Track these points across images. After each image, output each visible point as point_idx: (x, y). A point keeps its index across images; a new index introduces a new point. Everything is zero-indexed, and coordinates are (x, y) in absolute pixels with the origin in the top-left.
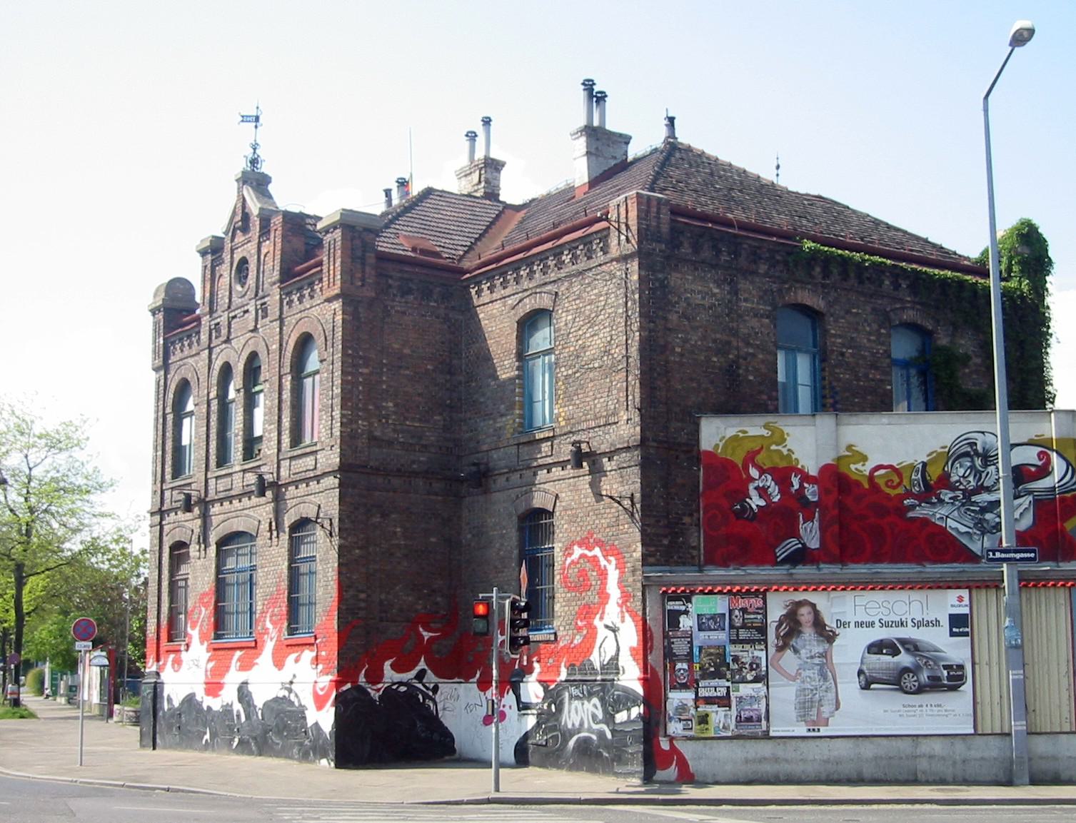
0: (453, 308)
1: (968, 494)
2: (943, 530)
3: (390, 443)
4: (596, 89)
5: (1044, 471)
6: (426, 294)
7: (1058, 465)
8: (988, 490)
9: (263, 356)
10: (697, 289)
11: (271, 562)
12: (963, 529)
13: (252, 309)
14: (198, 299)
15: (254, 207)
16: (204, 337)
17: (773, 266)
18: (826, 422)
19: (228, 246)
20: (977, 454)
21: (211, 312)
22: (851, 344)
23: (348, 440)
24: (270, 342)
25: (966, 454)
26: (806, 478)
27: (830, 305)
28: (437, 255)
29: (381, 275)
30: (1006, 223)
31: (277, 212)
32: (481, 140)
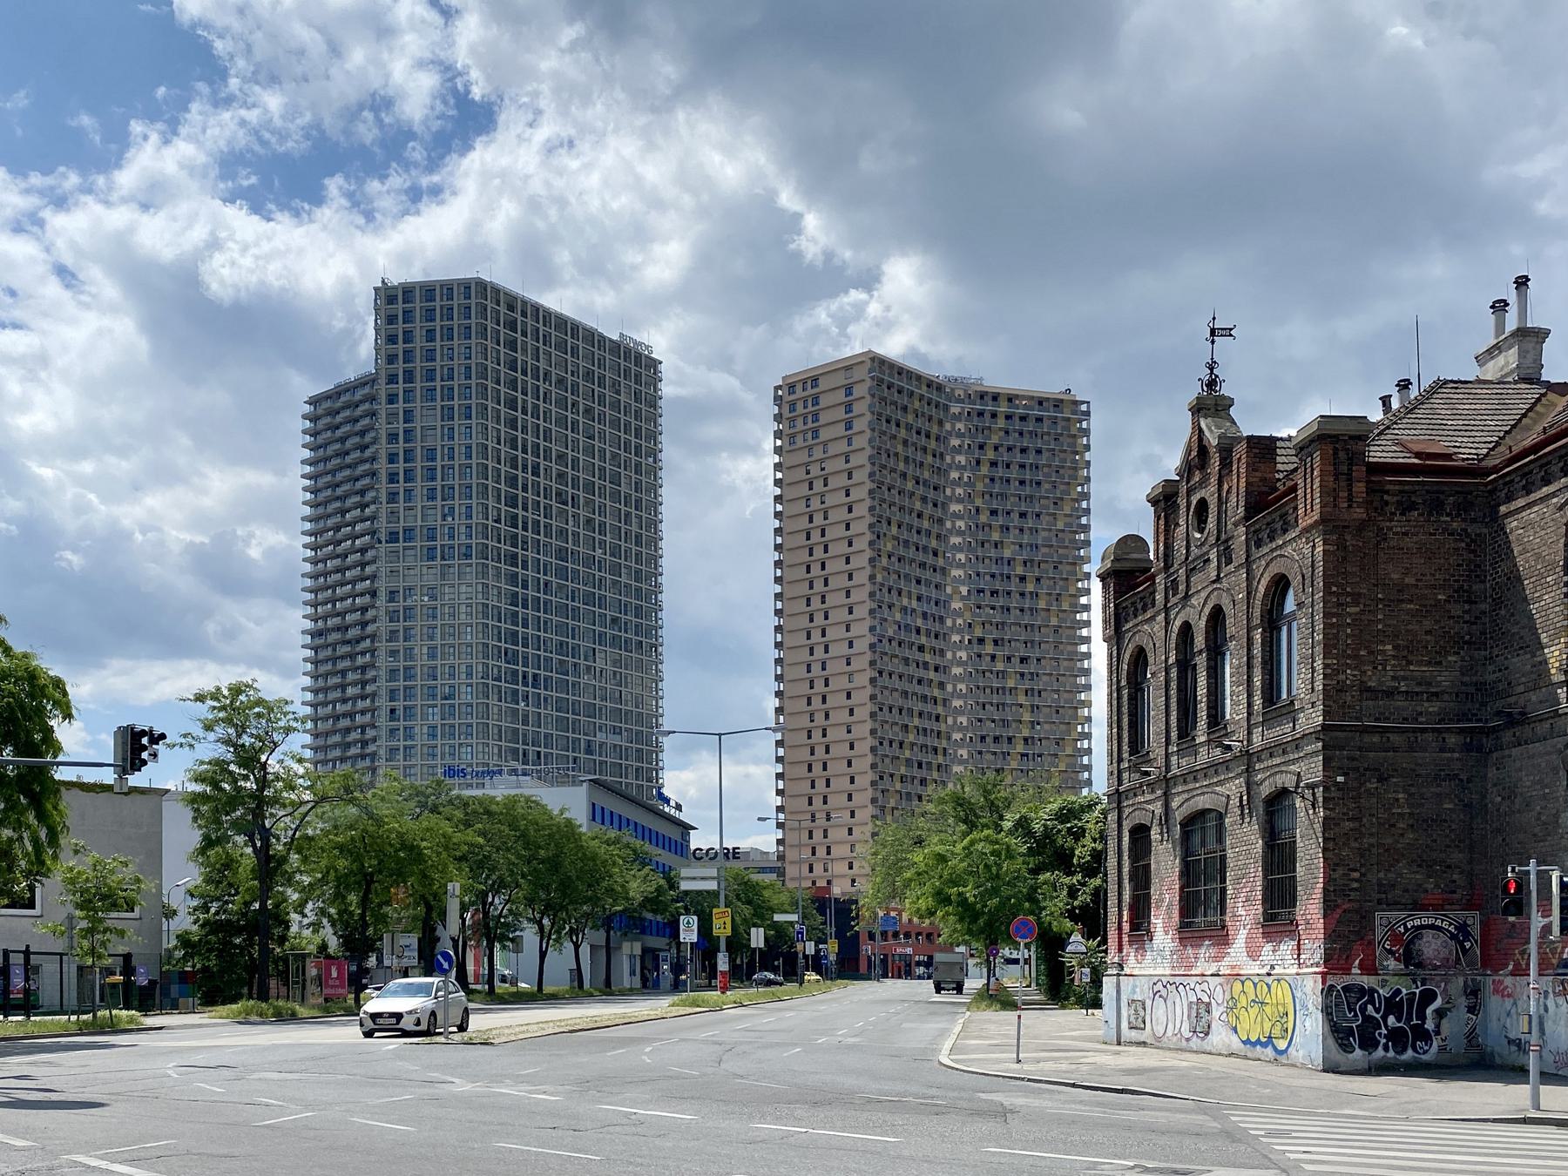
0: (1474, 521)
3: (1390, 694)
6: (1436, 506)
9: (1228, 609)
11: (1244, 846)
13: (1213, 555)
15: (1212, 439)
16: (1159, 597)
19: (1183, 489)
21: (1167, 567)
23: (1333, 696)
24: (1234, 593)
28: (1448, 457)
31: (1239, 439)
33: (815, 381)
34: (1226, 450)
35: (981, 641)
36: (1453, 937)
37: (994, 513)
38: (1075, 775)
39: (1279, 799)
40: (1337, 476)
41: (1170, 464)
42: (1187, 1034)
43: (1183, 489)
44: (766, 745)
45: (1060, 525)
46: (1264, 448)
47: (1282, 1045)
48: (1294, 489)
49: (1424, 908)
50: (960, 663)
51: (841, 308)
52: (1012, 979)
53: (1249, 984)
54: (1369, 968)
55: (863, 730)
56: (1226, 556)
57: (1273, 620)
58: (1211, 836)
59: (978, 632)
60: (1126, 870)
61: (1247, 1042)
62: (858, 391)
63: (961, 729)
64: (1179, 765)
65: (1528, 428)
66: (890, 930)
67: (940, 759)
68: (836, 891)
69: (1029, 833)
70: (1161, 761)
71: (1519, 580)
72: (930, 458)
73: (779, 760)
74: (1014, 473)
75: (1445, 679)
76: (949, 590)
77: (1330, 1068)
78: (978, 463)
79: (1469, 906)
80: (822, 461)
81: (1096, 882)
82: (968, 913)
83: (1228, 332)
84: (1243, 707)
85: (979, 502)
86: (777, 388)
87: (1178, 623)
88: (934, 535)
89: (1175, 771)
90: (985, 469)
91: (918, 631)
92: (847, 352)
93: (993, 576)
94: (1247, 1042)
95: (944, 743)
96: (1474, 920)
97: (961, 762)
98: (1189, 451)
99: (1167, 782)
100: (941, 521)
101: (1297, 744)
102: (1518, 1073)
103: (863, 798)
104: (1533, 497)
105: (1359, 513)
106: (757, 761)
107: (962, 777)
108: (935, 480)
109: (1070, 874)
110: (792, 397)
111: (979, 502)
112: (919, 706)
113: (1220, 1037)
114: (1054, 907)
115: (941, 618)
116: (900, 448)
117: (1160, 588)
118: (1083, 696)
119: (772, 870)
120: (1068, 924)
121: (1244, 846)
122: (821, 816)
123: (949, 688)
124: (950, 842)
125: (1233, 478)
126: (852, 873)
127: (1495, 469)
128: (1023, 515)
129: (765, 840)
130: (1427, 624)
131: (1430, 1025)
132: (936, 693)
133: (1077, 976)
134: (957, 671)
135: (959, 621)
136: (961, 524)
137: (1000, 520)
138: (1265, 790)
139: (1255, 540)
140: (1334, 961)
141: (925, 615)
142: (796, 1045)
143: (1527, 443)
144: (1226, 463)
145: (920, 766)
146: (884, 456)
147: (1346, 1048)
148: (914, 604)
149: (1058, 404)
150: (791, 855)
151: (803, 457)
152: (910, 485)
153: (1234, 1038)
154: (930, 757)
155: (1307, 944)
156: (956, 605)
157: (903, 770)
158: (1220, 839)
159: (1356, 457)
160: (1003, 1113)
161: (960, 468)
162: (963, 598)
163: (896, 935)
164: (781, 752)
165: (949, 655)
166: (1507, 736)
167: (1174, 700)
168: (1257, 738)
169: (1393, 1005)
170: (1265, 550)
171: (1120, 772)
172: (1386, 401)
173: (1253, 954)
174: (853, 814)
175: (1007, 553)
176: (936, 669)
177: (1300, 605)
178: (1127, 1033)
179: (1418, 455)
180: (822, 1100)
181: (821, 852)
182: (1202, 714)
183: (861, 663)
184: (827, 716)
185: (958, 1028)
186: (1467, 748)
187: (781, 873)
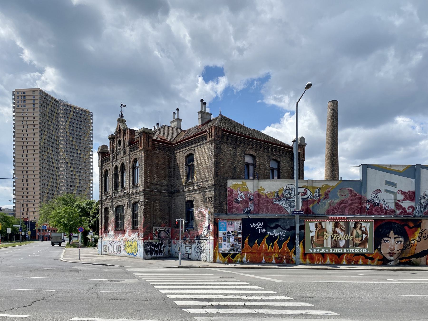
0: (170, 153)
1: (288, 199)
2: (282, 207)
3: (156, 184)
4: (204, 101)
5: (305, 194)
6: (164, 149)
7: (309, 193)
8: (292, 198)
9: (125, 164)
10: (227, 149)
11: (128, 213)
12: (286, 207)
13: (122, 152)
14: (109, 150)
15: (122, 127)
16: (111, 159)
17: (244, 144)
18: (256, 181)
19: (116, 137)
20: (290, 190)
21: (112, 153)
22: (261, 163)
23: (146, 183)
24: (127, 161)
25: (288, 189)
26: (250, 194)
27: (257, 154)
28: (166, 140)
29: (153, 144)
30: (299, 137)
31: (127, 129)
32: (176, 114)
33: (24, 92)
34: (125, 130)
35: (67, 163)
36: (166, 232)
37: (70, 133)
38: (89, 195)
39: (135, 204)
40: (146, 140)
41: (113, 130)
42: (116, 252)
43: (116, 137)
44: (11, 182)
45: (86, 139)
46: (132, 132)
47: (135, 254)
48: (138, 141)
49: (161, 227)
50: (62, 167)
51: (34, 75)
52: (75, 241)
53: (129, 242)
54: (152, 239)
55: (37, 181)
56: (125, 153)
57: (134, 167)
58: (121, 210)
59: (67, 161)
60: (103, 217)
61: (128, 254)
62: (36, 97)
63: (62, 183)
64: (115, 195)
65: (179, 137)
66: (44, 229)
67: (57, 189)
68: (30, 219)
69: (80, 208)
70: (111, 194)
71: (178, 165)
72: (55, 118)
73: (14, 186)
74: (75, 125)
75: (165, 183)
76: (60, 150)
77: (145, 258)
78: (67, 121)
79: (169, 227)
80: (26, 113)
81: (95, 219)
82: (65, 225)
83: (125, 106)
84: (128, 184)
85: (67, 130)
86: (13, 92)
87: (115, 165)
88: (56, 136)
89: (114, 197)
90: (68, 123)
91: (52, 158)
92: (36, 87)
93: (70, 148)
94: (128, 254)
95: (58, 186)
96: (170, 229)
97: (62, 190)
98: (117, 129)
99: (112, 199)
100: (58, 133)
101: (139, 193)
102: (177, 258)
103: (37, 197)
104: (180, 150)
105: (150, 148)
106: (8, 186)
107: (63, 193)
108: (56, 123)
109: (89, 217)
110: (18, 95)
111: (67, 130)
112: (52, 176)
113: (123, 253)
114: (86, 225)
115: (58, 156)
116: (47, 114)
117: (111, 157)
118: (91, 178)
119: (12, 214)
120: (89, 228)
121: (128, 213)
122: (26, 201)
123: (60, 173)
124: (62, 209)
125: (124, 137)
126: (35, 215)
127: (174, 144)
128: (77, 135)
129: (10, 206)
130: (163, 172)
131: (162, 250)
132: (56, 173)
133: (91, 240)
134: (61, 169)
135: (62, 157)
136: (62, 135)
137: (72, 136)
138: (132, 202)
139: (131, 150)
140: (145, 237)
141: (54, 155)
142: (22, 257)
143: (179, 140)
144: (125, 133)
145: (52, 190)
146: (43, 115)
147: (147, 254)
148: (51, 152)
149: (85, 112)
150: (17, 210)
151: (21, 111)
152: (50, 123)
153: (126, 253)
154: (55, 189)
155: (140, 234)
156: (61, 154)
157: (48, 191)
158: (123, 211)
159: (150, 137)
160: (78, 271)
161: (62, 121)
162: (63, 152)
163: (46, 230)
164: (15, 184)
165: (60, 165)
166: (176, 195)
167: (114, 182)
168: (131, 191)
169: (156, 246)
170: (133, 153)
171: (102, 196)
172: (154, 127)
173: (130, 236)
174: (34, 201)
175: (74, 143)
176: (56, 168)
177: (139, 165)
178: (103, 252)
179: (161, 139)
180: (32, 270)
181: (26, 210)
182: (120, 185)
183: (37, 164)
184: (28, 176)
185: (64, 252)
186: (169, 196)
187: (14, 214)
